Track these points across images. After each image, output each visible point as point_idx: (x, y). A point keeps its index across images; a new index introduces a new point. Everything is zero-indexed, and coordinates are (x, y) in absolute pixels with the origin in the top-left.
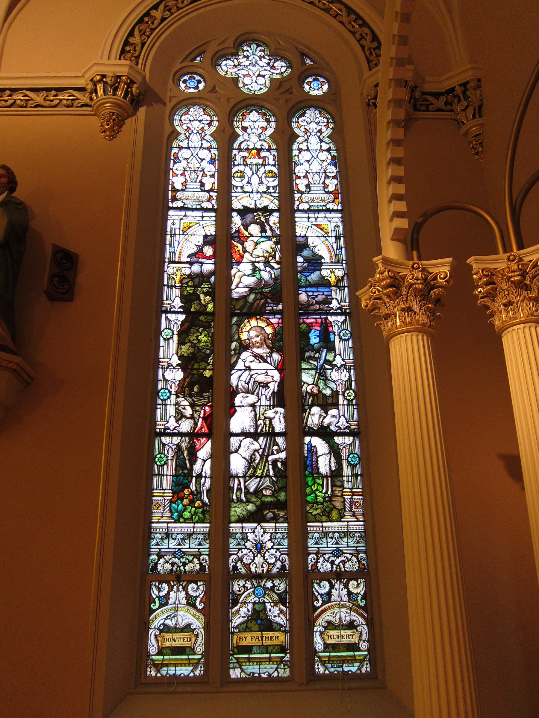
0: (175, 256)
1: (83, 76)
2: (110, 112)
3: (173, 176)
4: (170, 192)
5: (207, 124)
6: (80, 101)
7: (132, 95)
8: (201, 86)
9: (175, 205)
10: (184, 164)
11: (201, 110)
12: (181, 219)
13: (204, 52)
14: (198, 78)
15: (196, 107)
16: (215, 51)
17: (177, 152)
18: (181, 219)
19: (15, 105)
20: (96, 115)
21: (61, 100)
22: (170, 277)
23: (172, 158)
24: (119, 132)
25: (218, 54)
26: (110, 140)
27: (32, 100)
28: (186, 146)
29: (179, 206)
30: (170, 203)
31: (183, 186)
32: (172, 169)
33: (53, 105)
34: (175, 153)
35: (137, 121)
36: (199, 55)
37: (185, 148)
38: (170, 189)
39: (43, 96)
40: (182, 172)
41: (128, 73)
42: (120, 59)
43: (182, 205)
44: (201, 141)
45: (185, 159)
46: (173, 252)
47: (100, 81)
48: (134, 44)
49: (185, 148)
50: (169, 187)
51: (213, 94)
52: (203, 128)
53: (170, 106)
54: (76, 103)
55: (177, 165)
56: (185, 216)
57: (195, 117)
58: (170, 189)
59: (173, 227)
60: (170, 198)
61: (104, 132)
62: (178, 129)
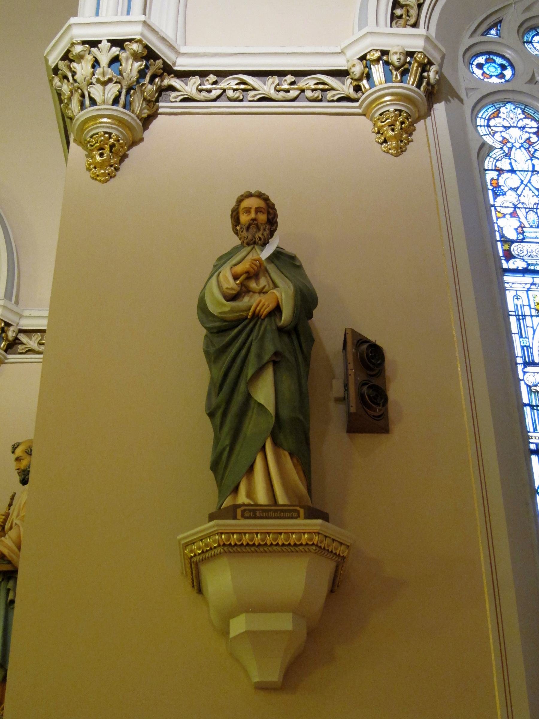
0: (532, 353)
1: (342, 52)
2: (106, 133)
3: (497, 218)
4: (499, 244)
5: (534, 133)
6: (334, 92)
7: (428, 83)
8: (508, 73)
9: (512, 264)
10: (511, 198)
11: (519, 111)
12: (529, 290)
13: (500, 22)
14: (499, 60)
15: (510, 106)
16: (521, 21)
17: (496, 177)
18: (529, 290)
19: (222, 97)
20: (364, 115)
21: (303, 91)
22: (531, 391)
23: (490, 187)
24: (409, 142)
25: (526, 25)
26: (397, 155)
27: (254, 89)
28: (509, 168)
29: (520, 268)
30: (504, 262)
31: (518, 234)
32: (493, 206)
33: (289, 98)
34: (492, 179)
35: (434, 124)
36: (494, 25)
37: (508, 171)
38: (498, 238)
39: (273, 83)
40: (511, 210)
41: (424, 48)
42: (391, 27)
43: (525, 266)
44: (531, 160)
45: (511, 189)
46: (527, 347)
47: (378, 60)
48: (407, 5)
49: (508, 171)
50: (495, 236)
51: (532, 86)
52: (529, 139)
53: (469, 103)
54: (329, 95)
55: (500, 200)
56: (533, 284)
57: (511, 122)
58: (498, 238)
59: (519, 303)
60: (501, 254)
61: (385, 141)
62: (488, 140)
